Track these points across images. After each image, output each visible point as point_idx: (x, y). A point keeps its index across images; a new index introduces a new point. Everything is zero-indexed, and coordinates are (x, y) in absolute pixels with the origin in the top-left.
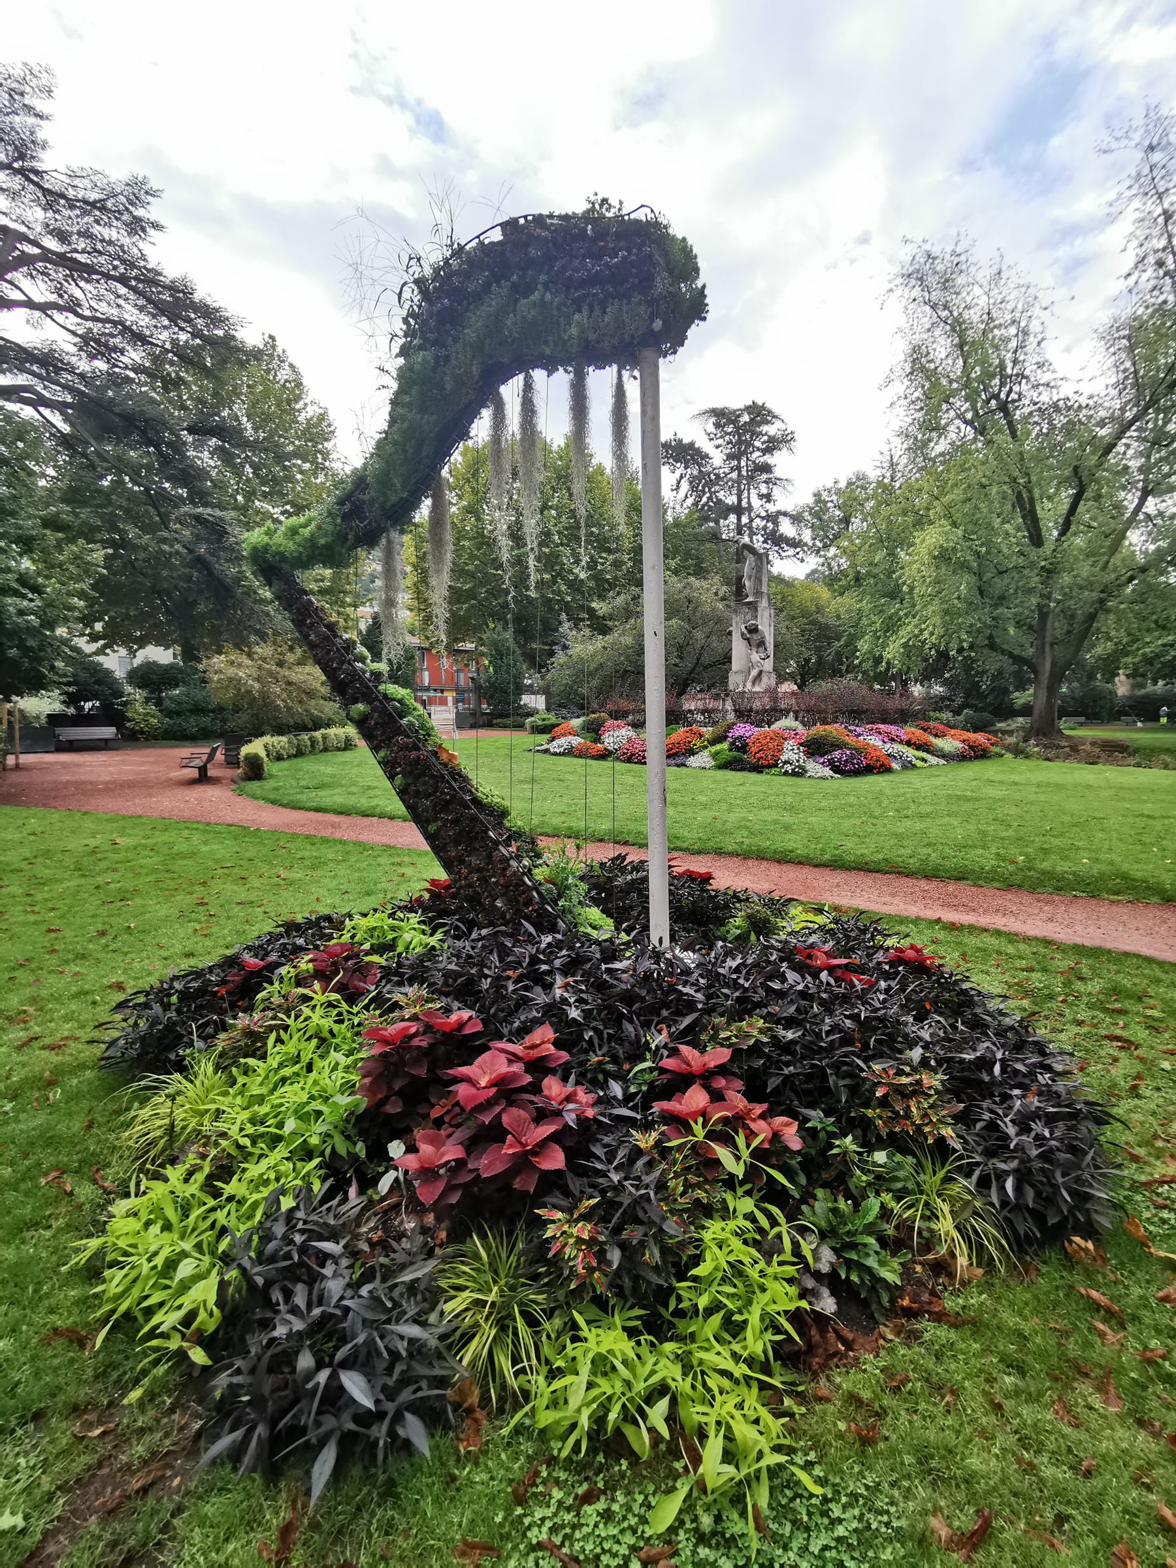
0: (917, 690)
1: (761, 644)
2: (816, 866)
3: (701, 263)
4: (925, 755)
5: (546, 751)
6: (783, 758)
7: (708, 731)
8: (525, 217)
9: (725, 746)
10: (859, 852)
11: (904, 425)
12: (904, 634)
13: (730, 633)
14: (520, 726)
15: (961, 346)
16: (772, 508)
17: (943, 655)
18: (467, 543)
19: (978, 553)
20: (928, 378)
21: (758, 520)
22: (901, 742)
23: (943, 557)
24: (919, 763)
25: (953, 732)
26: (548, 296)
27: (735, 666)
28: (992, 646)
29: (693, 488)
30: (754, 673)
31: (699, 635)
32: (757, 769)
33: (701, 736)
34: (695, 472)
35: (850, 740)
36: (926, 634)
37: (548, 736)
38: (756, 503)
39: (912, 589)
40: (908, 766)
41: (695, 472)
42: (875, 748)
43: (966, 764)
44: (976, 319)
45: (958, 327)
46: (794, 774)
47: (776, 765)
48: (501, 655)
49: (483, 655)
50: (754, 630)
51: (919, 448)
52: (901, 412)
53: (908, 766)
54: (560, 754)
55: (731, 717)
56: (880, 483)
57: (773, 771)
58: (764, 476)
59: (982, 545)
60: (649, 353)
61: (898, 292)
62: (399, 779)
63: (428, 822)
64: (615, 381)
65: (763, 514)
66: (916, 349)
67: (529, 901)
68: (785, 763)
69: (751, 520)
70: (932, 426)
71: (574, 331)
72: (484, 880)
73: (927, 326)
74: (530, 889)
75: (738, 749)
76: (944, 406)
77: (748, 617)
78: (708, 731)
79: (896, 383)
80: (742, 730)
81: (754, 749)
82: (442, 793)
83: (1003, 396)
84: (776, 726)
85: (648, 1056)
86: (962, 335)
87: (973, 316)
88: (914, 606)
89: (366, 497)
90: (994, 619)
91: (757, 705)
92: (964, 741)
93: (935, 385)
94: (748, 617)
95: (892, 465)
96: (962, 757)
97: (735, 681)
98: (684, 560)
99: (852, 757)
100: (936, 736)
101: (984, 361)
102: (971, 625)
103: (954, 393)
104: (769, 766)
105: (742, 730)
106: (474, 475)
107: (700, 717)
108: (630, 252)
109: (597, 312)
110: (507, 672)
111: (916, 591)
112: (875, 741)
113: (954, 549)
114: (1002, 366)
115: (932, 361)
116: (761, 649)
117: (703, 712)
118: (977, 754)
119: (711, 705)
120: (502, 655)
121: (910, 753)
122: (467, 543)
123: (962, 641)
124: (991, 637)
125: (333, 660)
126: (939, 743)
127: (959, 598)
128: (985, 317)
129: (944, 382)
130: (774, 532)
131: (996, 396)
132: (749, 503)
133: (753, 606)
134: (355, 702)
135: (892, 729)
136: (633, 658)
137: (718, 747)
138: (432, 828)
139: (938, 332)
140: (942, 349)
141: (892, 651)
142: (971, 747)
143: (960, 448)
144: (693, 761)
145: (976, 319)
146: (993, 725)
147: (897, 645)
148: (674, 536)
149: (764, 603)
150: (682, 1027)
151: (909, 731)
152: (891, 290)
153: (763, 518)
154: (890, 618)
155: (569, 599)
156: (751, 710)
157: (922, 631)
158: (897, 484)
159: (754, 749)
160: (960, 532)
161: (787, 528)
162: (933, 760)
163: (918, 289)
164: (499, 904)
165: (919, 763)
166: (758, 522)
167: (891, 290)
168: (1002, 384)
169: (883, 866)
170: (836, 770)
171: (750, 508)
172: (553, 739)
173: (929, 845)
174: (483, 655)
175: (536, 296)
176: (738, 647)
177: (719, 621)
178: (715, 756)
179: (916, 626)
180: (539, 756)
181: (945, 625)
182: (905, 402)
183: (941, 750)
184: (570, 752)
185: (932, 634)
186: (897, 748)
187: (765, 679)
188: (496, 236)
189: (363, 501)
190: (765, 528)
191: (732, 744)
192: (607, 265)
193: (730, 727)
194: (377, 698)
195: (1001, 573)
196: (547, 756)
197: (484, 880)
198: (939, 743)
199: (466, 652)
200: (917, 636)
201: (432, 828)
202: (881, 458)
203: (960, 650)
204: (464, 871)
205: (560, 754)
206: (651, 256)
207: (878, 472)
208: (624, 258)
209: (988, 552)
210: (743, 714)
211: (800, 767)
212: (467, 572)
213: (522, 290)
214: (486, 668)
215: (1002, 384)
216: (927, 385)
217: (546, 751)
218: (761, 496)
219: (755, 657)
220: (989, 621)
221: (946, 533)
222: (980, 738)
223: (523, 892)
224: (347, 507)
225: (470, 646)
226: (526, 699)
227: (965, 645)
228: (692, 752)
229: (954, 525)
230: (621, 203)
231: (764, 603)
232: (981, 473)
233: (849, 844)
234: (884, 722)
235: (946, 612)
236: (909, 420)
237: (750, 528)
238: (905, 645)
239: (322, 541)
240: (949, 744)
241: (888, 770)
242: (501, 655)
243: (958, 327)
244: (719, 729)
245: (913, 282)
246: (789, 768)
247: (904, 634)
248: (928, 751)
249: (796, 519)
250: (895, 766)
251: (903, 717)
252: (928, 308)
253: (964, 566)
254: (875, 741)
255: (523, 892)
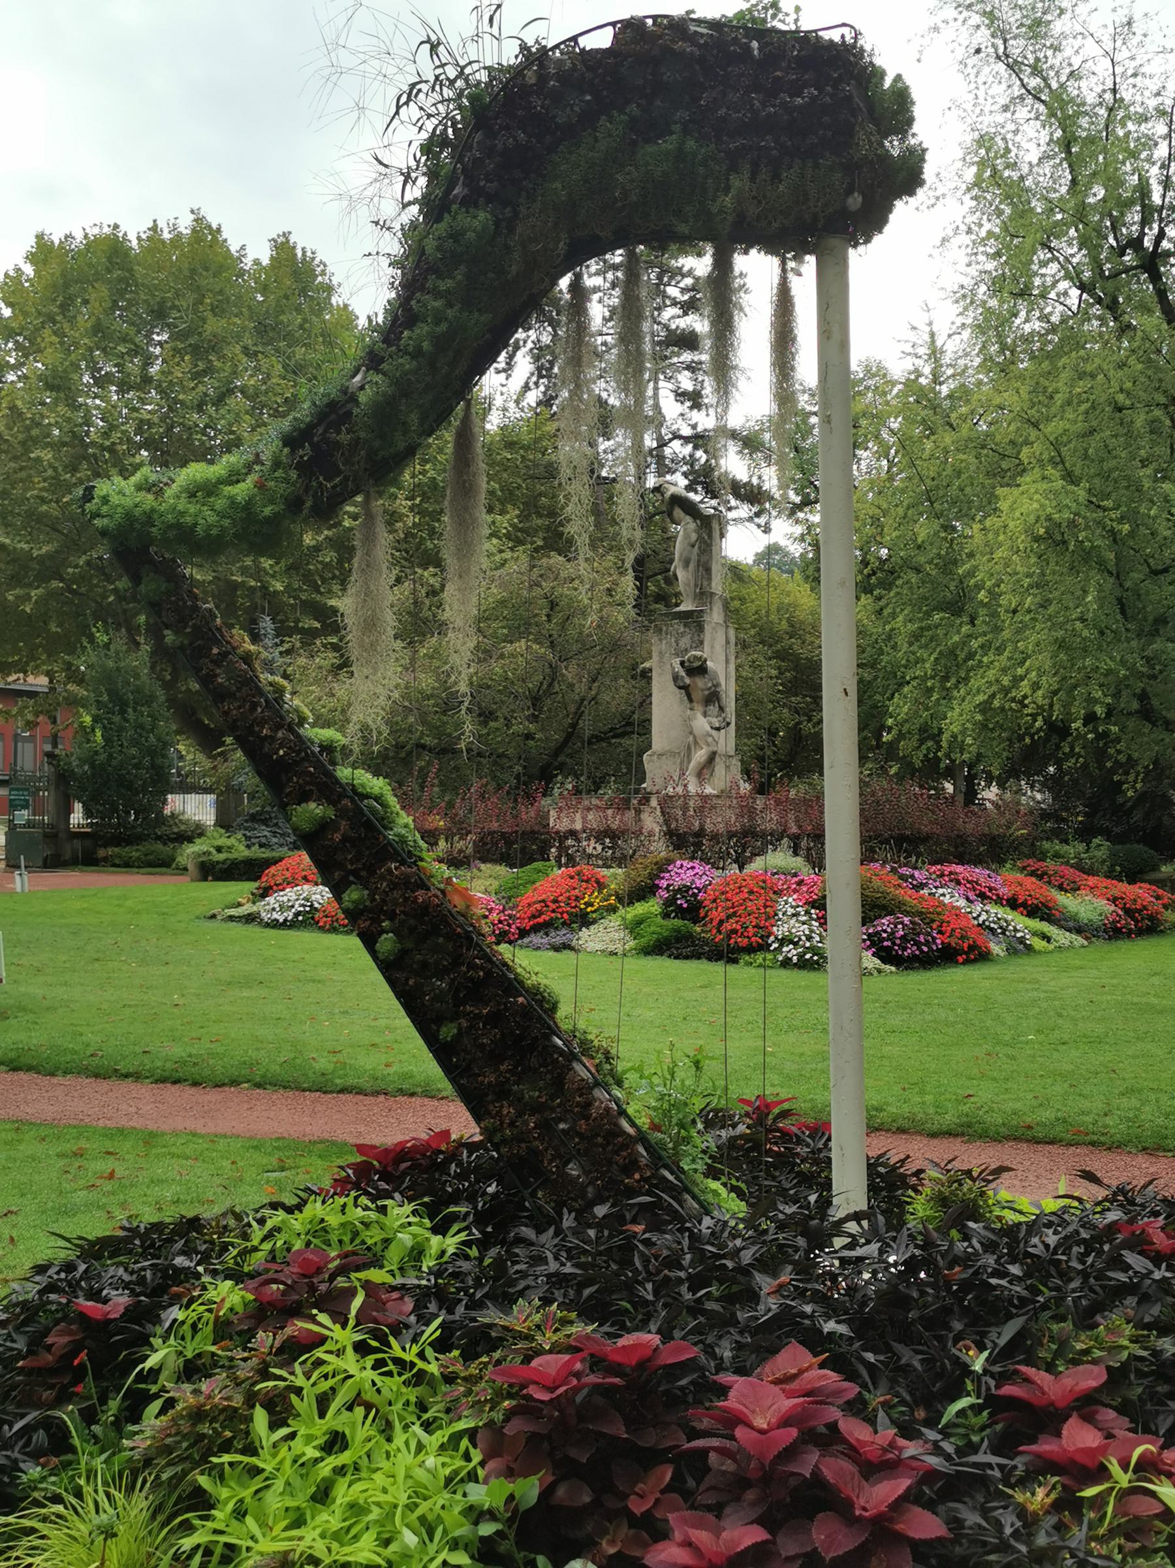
0: (990, 793)
1: (713, 698)
2: (933, 1135)
3: (917, 111)
4: (1045, 927)
5: (251, 918)
6: (780, 931)
7: (615, 877)
8: (655, 17)
9: (651, 907)
10: (1010, 1106)
11: (968, 282)
12: (981, 685)
13: (646, 675)
14: (163, 864)
15: (1066, 144)
16: (705, 421)
17: (1058, 730)
18: (47, 455)
19: (1113, 533)
20: (1007, 197)
21: (676, 445)
22: (999, 901)
23: (1052, 539)
24: (1038, 944)
25: (1092, 880)
26: (691, 144)
27: (659, 740)
28: (1147, 713)
29: (542, 371)
30: (700, 756)
31: (569, 672)
32: (726, 954)
33: (600, 885)
34: (546, 339)
35: (905, 894)
36: (1025, 687)
37: (252, 886)
38: (671, 408)
39: (994, 595)
40: (1019, 948)
41: (546, 339)
42: (957, 913)
43: (1124, 945)
44: (1091, 98)
45: (1060, 108)
46: (803, 964)
47: (764, 947)
48: (120, 703)
49: (74, 702)
50: (698, 669)
51: (992, 326)
52: (962, 257)
53: (1019, 948)
54: (284, 925)
55: (660, 848)
56: (911, 384)
57: (759, 957)
58: (687, 357)
59: (1121, 520)
60: (834, 241)
61: (948, 33)
62: (387, 943)
63: (440, 1020)
64: (776, 280)
65: (686, 431)
66: (984, 141)
67: (632, 1165)
68: (783, 941)
69: (662, 444)
70: (1015, 286)
71: (728, 201)
72: (546, 1126)
73: (1004, 100)
74: (630, 1141)
75: (681, 913)
76: (1043, 255)
77: (685, 642)
78: (615, 877)
79: (951, 201)
80: (687, 873)
81: (717, 914)
82: (472, 966)
83: (1148, 243)
84: (757, 865)
85: (970, 1386)
86: (1067, 123)
87: (1089, 91)
88: (998, 629)
89: (344, 438)
90: (1148, 660)
91: (716, 822)
92: (1114, 900)
93: (1023, 213)
94: (685, 642)
95: (935, 354)
96: (1114, 932)
97: (657, 770)
98: (523, 517)
99: (914, 930)
100: (1061, 888)
101: (1114, 182)
102: (1109, 672)
103: (1056, 231)
104: (751, 950)
105: (687, 873)
106: (64, 308)
107: (593, 847)
108: (820, 89)
109: (764, 175)
110: (135, 743)
111: (1003, 601)
112: (952, 898)
113: (1072, 524)
114: (1143, 190)
115: (1013, 166)
116: (713, 709)
117: (600, 836)
118: (1135, 925)
119: (615, 821)
120: (123, 705)
121: (1020, 922)
122: (47, 455)
123: (1090, 700)
124: (1143, 697)
125: (262, 722)
126: (1067, 902)
127: (1082, 620)
128: (1108, 96)
129: (1038, 207)
130: (708, 470)
131: (1136, 243)
132: (657, 407)
133: (694, 621)
134: (304, 798)
135: (979, 873)
136: (435, 719)
137: (640, 909)
138: (448, 1032)
139: (1022, 113)
140: (1032, 142)
141: (958, 719)
142: (1128, 911)
143: (1068, 335)
144: (591, 938)
145: (1091, 98)
146: (1155, 868)
147: (967, 706)
148: (505, 466)
149: (715, 616)
150: (1002, 1342)
151: (1008, 878)
152: (936, 29)
153: (686, 440)
154: (952, 653)
155: (279, 587)
156: (701, 833)
157: (1016, 680)
158: (944, 390)
159: (717, 914)
160: (1082, 494)
161: (734, 465)
162: (1062, 937)
163: (985, 32)
164: (573, 1170)
165: (1038, 944)
166: (677, 448)
167: (936, 29)
168: (1145, 222)
169: (1058, 1131)
170: (886, 955)
171: (658, 419)
172: (265, 893)
173: (1129, 1092)
174: (74, 702)
175: (668, 144)
176: (665, 705)
177: (615, 647)
178: (634, 927)
179: (1004, 670)
180: (238, 929)
181: (1057, 667)
182: (966, 239)
183: (1074, 918)
184: (308, 920)
185: (1036, 686)
186: (997, 912)
187: (719, 767)
188: (603, 40)
189: (337, 445)
190: (692, 460)
191: (669, 902)
192: (784, 104)
193: (662, 867)
194: (342, 796)
195: (1156, 573)
196: (253, 930)
197: (546, 1126)
198: (1067, 902)
199: (32, 694)
200: (1006, 691)
201: (448, 1032)
202: (912, 336)
203: (1090, 718)
204: (508, 1111)
205: (284, 925)
206: (849, 98)
207: (908, 364)
208: (813, 99)
209: (1132, 534)
210: (685, 841)
211: (812, 949)
212: (40, 518)
213: (651, 129)
214: (86, 733)
215: (1145, 222)
216: (1008, 211)
217: (251, 918)
218: (681, 395)
219: (702, 724)
220: (1140, 665)
221: (1056, 494)
222: (1141, 893)
223: (624, 1146)
224: (306, 452)
225: (39, 682)
226: (175, 803)
227: (1099, 710)
228: (585, 920)
229: (1070, 477)
230: (798, 9)
231: (715, 616)
232: (1115, 385)
233: (985, 1093)
234: (961, 862)
235: (1062, 645)
236: (973, 271)
237: (660, 458)
238: (984, 708)
239: (267, 511)
240: (1088, 905)
241: (980, 956)
242: (120, 703)
243: (1060, 108)
244: (639, 872)
245: (976, 19)
246: (790, 951)
247: (981, 685)
248: (1048, 918)
249: (750, 443)
250: (996, 949)
251: (994, 850)
252: (1001, 67)
253: (1087, 556)
254: (952, 898)
255: (624, 1146)
